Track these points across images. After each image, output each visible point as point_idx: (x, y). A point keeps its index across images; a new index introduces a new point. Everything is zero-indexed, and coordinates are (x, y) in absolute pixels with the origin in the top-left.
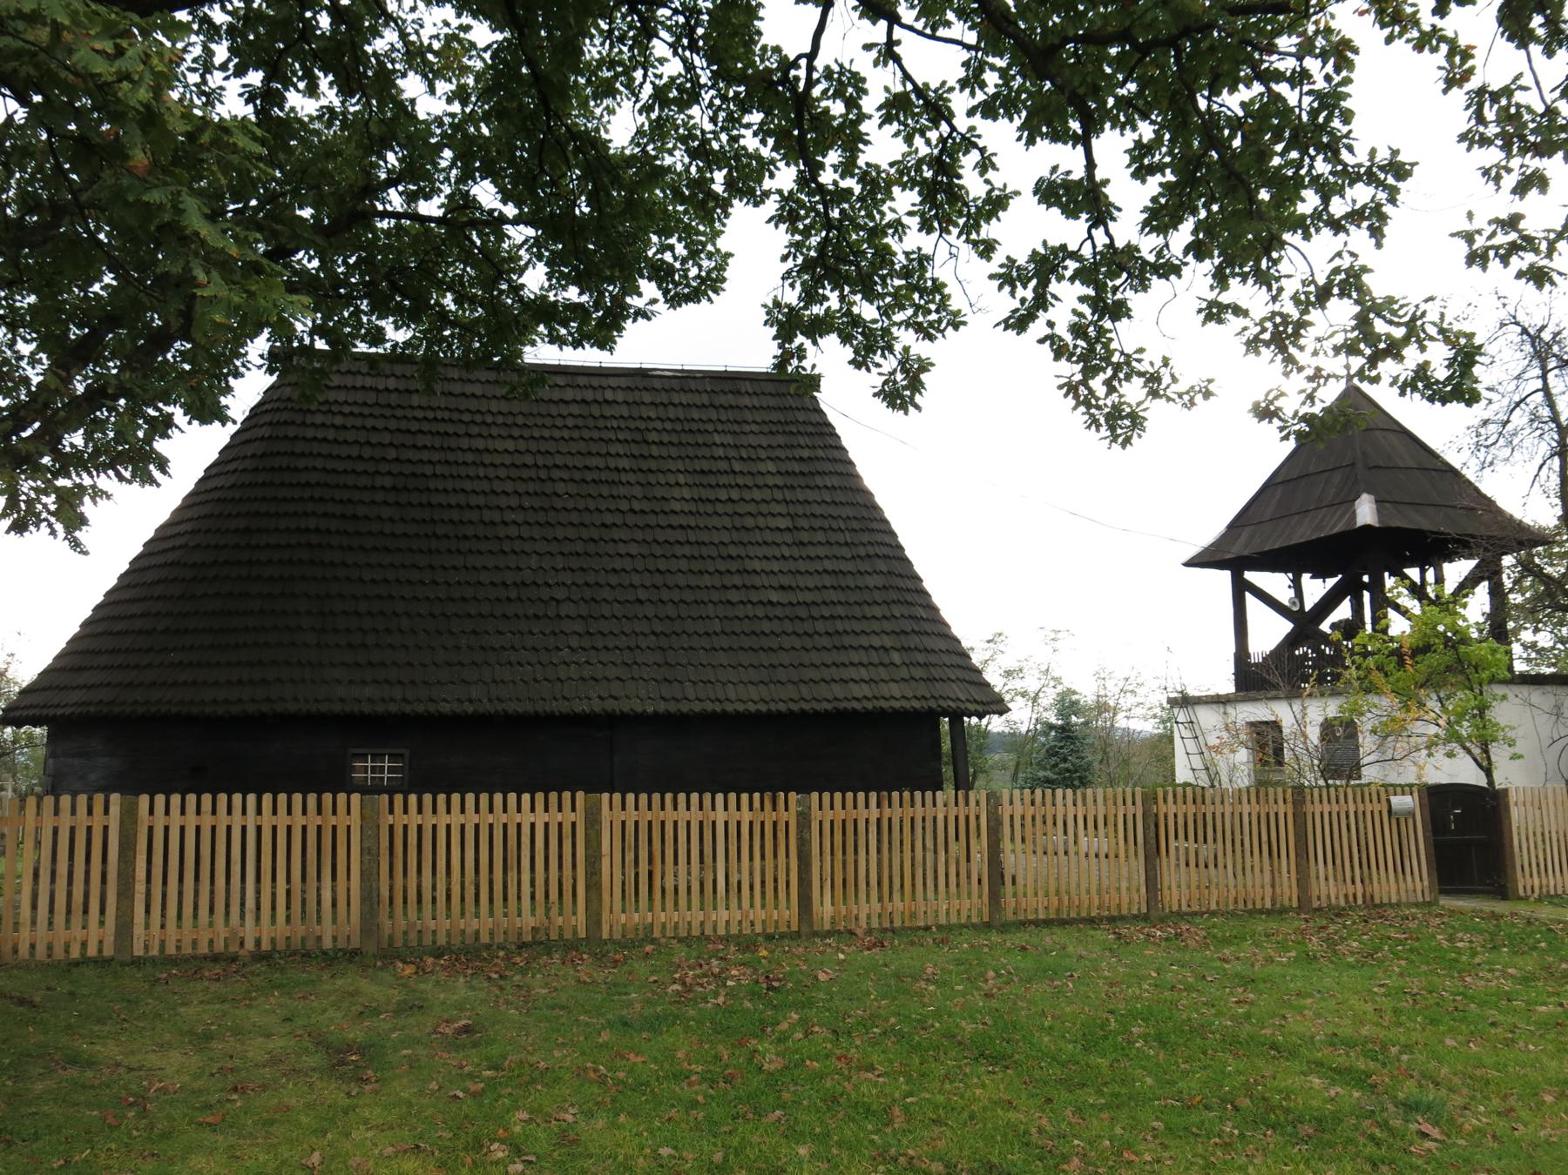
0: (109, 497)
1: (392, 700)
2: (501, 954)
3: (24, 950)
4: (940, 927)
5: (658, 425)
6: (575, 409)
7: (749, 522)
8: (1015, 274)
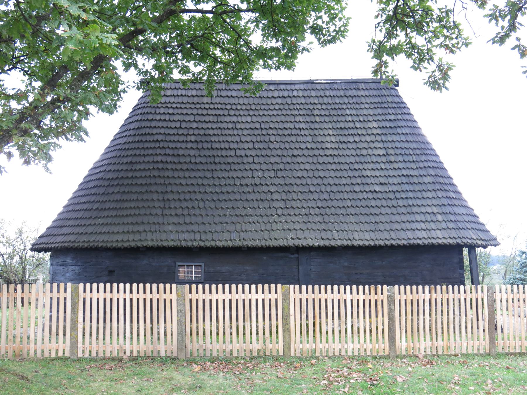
0: (61, 147)
1: (195, 240)
2: (242, 361)
3: (32, 353)
4: (463, 355)
5: (319, 107)
6: (279, 101)
7: (364, 152)
8: (498, 14)
